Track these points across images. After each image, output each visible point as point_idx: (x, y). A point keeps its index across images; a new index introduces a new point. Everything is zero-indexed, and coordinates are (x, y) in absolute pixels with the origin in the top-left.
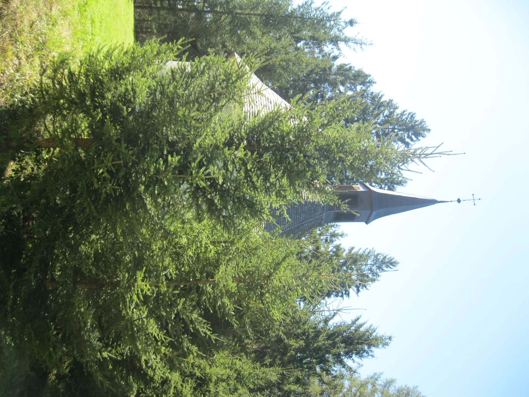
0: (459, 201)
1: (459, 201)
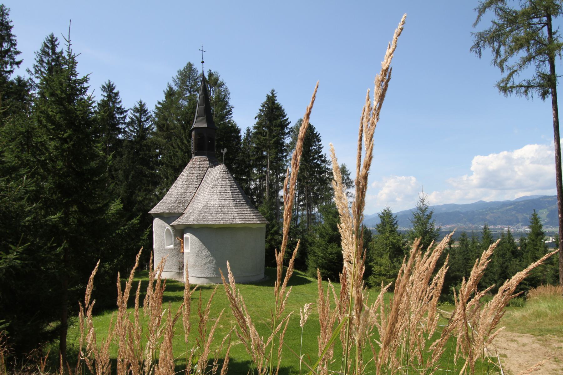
0: (203, 62)
1: (203, 62)
